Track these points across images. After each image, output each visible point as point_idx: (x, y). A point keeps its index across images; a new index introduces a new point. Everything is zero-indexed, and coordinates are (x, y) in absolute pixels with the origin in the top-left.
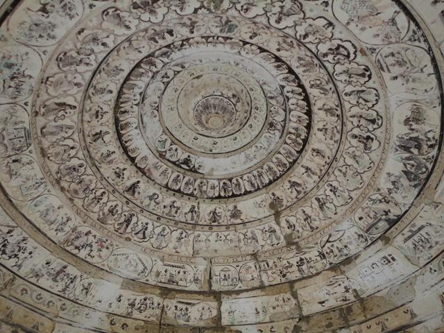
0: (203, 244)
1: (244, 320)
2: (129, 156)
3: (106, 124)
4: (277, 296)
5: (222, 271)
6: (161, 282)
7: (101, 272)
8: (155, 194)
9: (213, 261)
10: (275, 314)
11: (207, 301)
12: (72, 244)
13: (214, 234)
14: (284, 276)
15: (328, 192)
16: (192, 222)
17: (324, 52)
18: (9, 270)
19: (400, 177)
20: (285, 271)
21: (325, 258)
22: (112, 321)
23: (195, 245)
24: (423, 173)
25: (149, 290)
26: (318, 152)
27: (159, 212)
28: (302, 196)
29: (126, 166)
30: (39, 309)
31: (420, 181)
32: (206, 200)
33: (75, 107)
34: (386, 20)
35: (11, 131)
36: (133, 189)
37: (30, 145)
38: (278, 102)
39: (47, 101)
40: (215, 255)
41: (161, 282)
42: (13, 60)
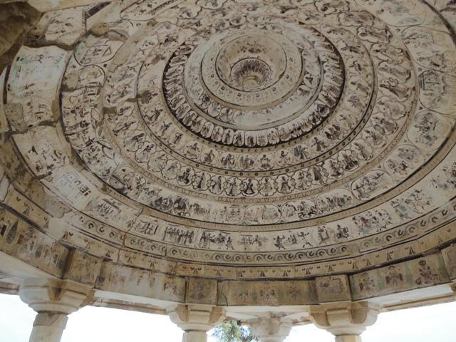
15: (146, 144)
19: (157, 195)
20: (78, 111)
21: (88, 145)
26: (179, 138)
28: (145, 121)
33: (381, 86)
37: (420, 76)
38: (223, 115)
42: (426, 141)
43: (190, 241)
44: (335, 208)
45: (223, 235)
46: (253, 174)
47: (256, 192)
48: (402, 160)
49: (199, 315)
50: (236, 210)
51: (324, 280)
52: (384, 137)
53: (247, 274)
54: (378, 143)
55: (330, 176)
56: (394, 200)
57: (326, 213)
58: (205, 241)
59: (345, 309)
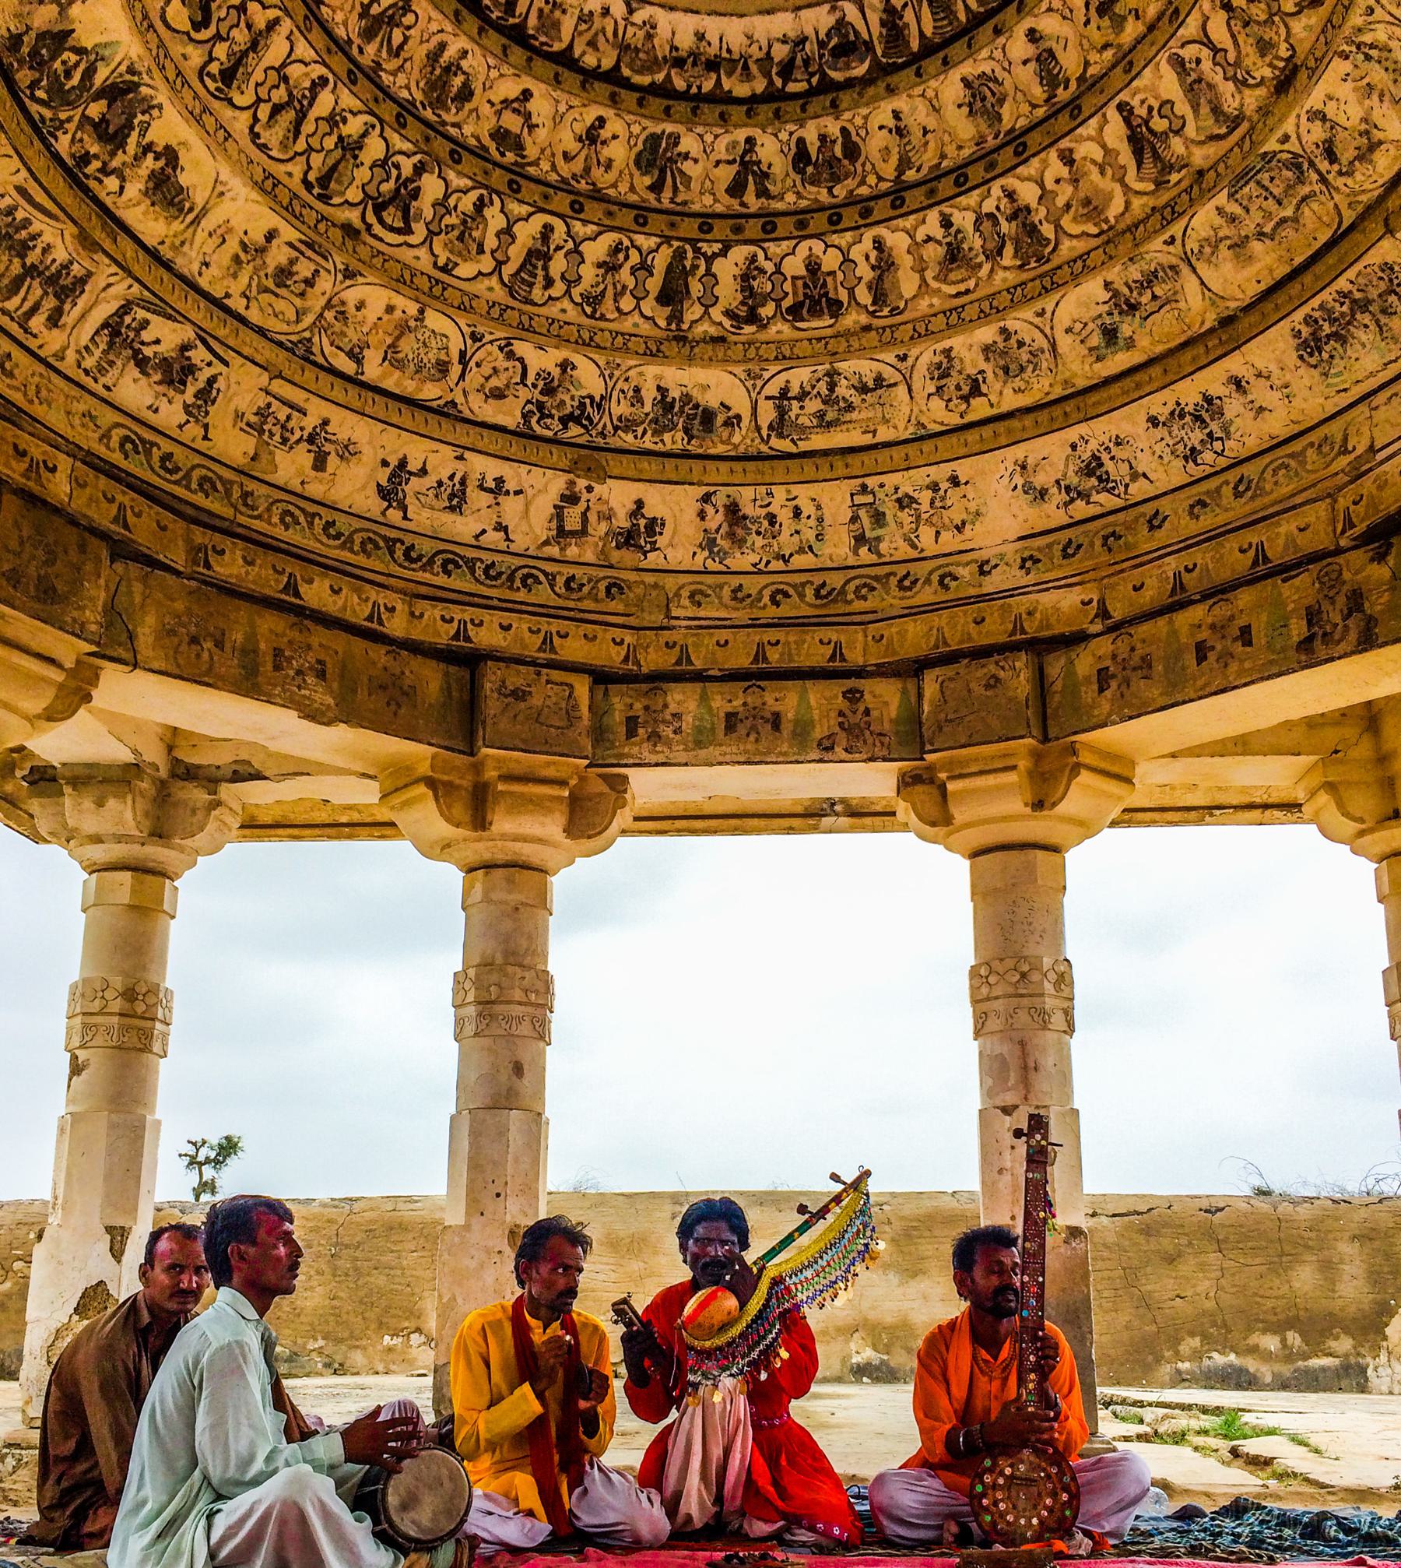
17: (425, 176)
24: (34, 85)
31: (21, 62)
33: (1120, 107)
34: (366, 352)
35: (1257, 216)
42: (1096, 340)
43: (54, 321)
44: (667, 437)
45: (199, 355)
46: (442, 148)
47: (420, 231)
48: (983, 365)
49: (16, 669)
50: (304, 269)
51: (517, 677)
52: (987, 267)
53: (231, 566)
54: (953, 276)
55: (716, 313)
56: (872, 482)
57: (628, 440)
58: (111, 344)
59: (562, 783)
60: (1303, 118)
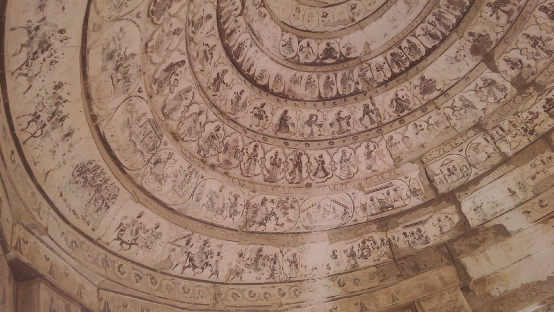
0: (401, 146)
1: (498, 209)
2: (259, 86)
3: (220, 61)
4: (532, 162)
5: (442, 165)
6: (372, 215)
7: (299, 237)
8: (311, 116)
9: (424, 160)
10: (539, 184)
11: (440, 210)
12: (254, 222)
13: (411, 127)
14: (532, 132)
16: (373, 126)
18: (207, 282)
20: (530, 126)
22: (339, 283)
23: (391, 152)
25: (363, 230)
27: (327, 133)
29: (263, 101)
30: (261, 306)
32: (378, 89)
33: (183, 62)
35: (137, 132)
36: (283, 123)
39: (155, 73)
40: (422, 151)
41: (372, 215)
60: (171, 151)
